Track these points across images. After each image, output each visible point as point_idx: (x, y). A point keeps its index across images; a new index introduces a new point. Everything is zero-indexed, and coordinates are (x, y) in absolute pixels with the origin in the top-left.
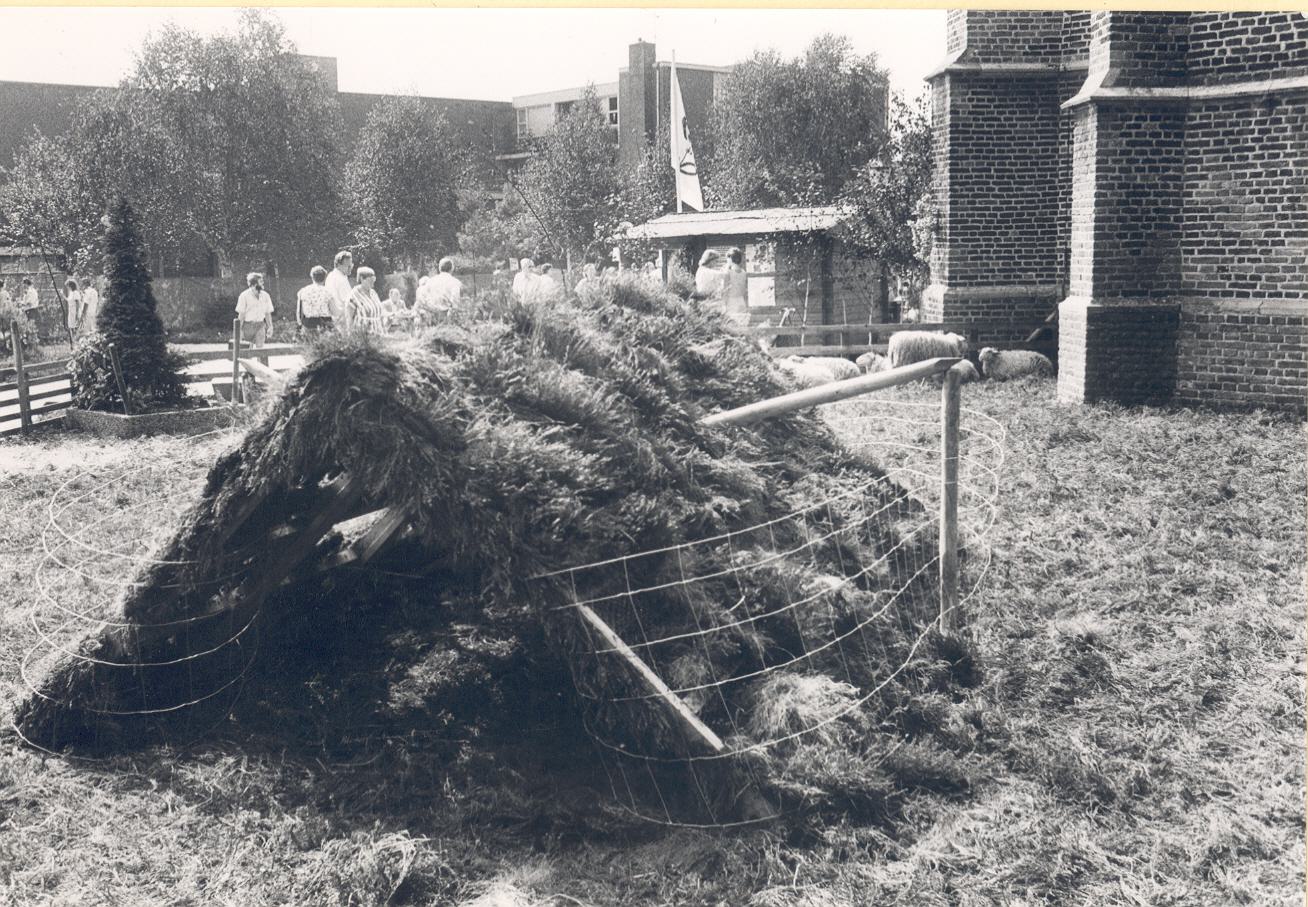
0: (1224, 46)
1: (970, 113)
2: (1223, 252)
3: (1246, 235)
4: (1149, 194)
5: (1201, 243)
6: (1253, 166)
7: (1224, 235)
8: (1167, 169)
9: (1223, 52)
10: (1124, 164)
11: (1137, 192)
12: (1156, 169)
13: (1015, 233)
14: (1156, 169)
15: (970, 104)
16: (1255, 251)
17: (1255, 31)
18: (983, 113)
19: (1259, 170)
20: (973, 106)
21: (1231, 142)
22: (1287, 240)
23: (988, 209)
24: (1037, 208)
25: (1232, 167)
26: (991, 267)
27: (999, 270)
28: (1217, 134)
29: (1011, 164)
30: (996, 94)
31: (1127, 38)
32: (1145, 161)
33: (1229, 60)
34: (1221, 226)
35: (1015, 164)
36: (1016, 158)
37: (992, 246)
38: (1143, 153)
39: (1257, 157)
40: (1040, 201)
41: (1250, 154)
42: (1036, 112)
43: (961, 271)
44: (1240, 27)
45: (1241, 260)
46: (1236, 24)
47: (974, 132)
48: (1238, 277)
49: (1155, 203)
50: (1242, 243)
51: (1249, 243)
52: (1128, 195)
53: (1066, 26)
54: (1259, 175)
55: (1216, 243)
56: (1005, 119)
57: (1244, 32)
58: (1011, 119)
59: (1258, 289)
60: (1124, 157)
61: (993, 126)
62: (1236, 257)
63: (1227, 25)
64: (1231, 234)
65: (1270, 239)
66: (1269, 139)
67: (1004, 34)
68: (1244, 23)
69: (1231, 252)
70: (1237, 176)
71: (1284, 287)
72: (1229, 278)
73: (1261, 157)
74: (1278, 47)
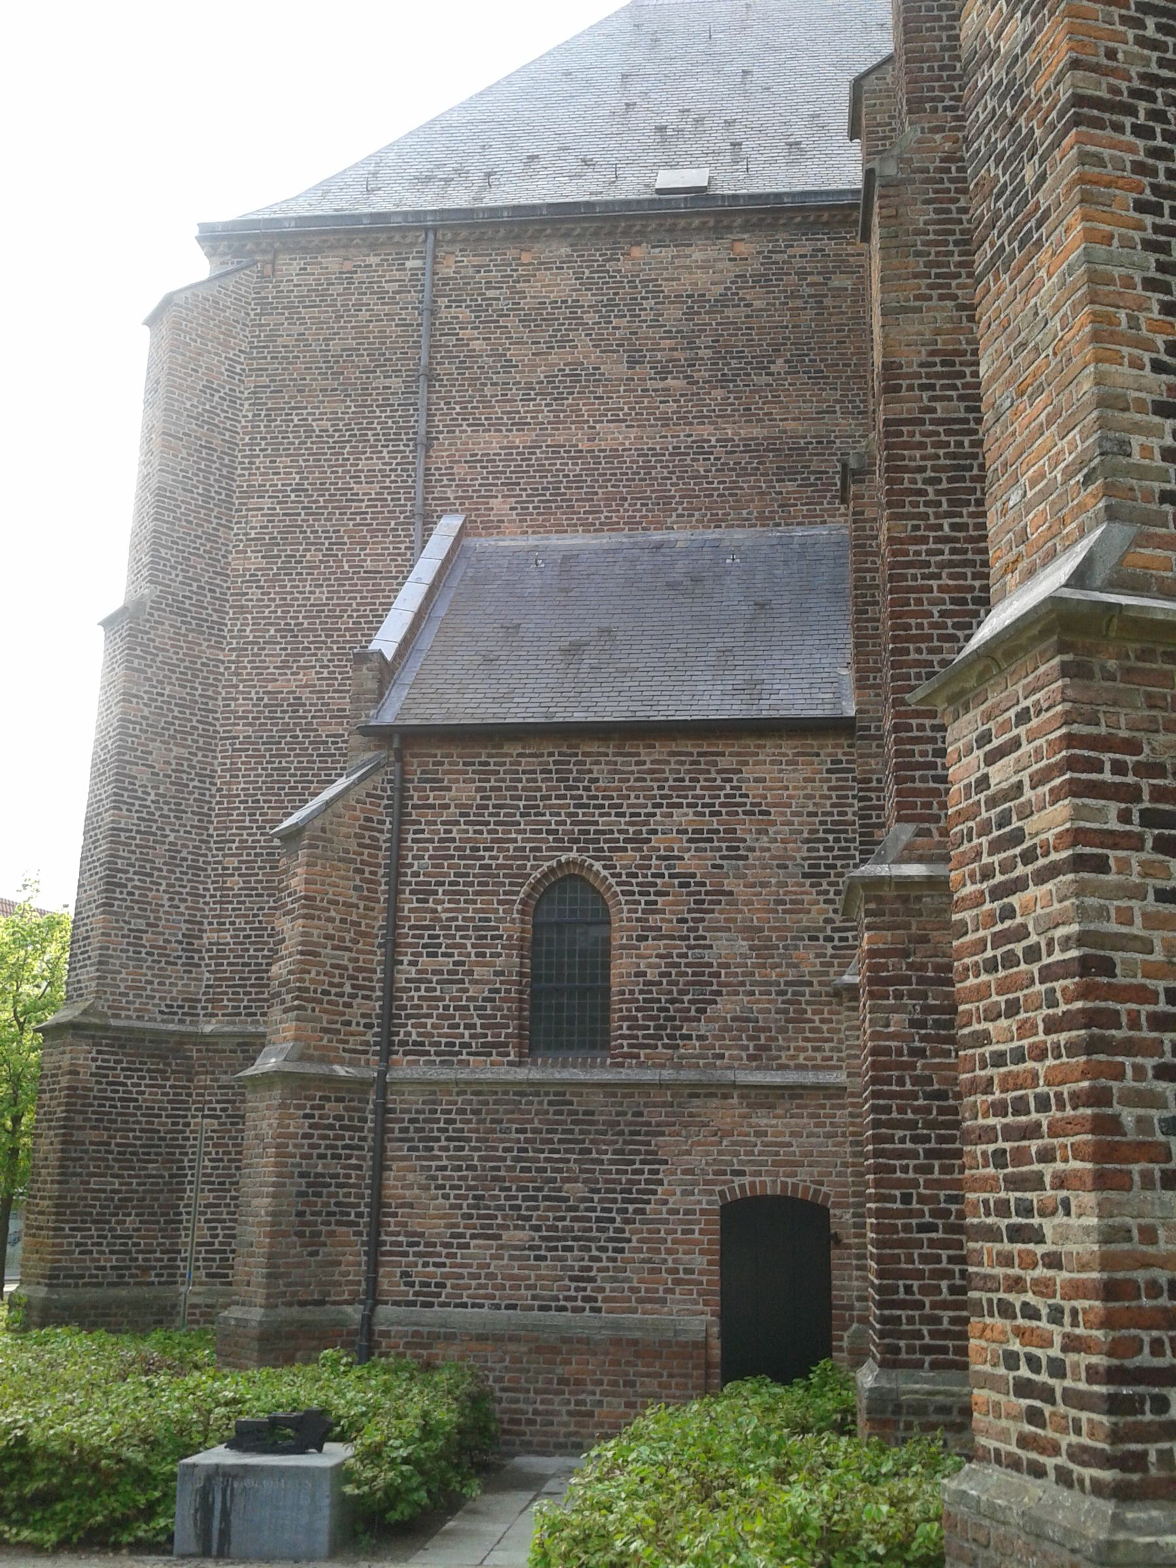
0: (409, 1028)
1: (92, 1075)
2: (406, 1254)
3: (431, 1235)
4: (330, 1185)
5: (224, 1221)
6: (439, 1158)
7: (408, 1234)
8: (349, 1157)
9: (409, 1034)
10: (306, 1150)
11: (316, 1183)
12: (339, 1157)
13: (133, 1222)
14: (339, 1157)
15: (94, 1065)
16: (439, 1255)
17: (439, 1017)
18: (107, 1076)
19: (445, 1163)
20: (98, 1067)
21: (417, 1130)
22: (473, 1242)
23: (104, 1191)
24: (162, 1191)
25: (418, 1158)
26: (102, 1263)
27: (112, 1268)
28: (403, 1121)
29: (135, 1138)
30: (124, 1054)
31: (313, 1010)
32: (327, 1147)
33: (415, 1043)
34: (405, 1224)
35: (140, 1138)
36: (142, 1131)
37: (105, 1237)
38: (326, 1137)
39: (442, 1149)
40: (165, 1184)
41: (436, 1145)
42: (168, 1079)
43: (66, 1268)
44: (425, 1011)
45: (426, 1265)
46: (421, 1007)
47: (95, 1098)
48: (423, 1284)
49: (336, 1195)
50: (427, 1245)
51: (434, 1245)
52: (309, 1185)
53: (207, 986)
54: (444, 1168)
55: (400, 1244)
56: (133, 1085)
57: (430, 1016)
58: (139, 1085)
59: (443, 1299)
60: (305, 1142)
61: (117, 1092)
62: (420, 1262)
63: (412, 1007)
64: (414, 1234)
65: (455, 1241)
66: (454, 1130)
67: (139, 988)
68: (429, 1007)
69: (415, 1254)
70: (423, 1168)
71: (469, 1297)
72: (412, 1284)
73: (446, 1149)
74: (463, 1036)
